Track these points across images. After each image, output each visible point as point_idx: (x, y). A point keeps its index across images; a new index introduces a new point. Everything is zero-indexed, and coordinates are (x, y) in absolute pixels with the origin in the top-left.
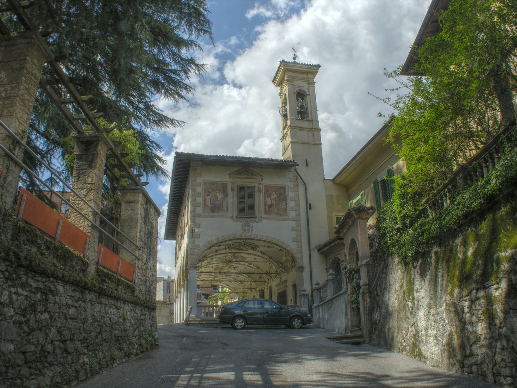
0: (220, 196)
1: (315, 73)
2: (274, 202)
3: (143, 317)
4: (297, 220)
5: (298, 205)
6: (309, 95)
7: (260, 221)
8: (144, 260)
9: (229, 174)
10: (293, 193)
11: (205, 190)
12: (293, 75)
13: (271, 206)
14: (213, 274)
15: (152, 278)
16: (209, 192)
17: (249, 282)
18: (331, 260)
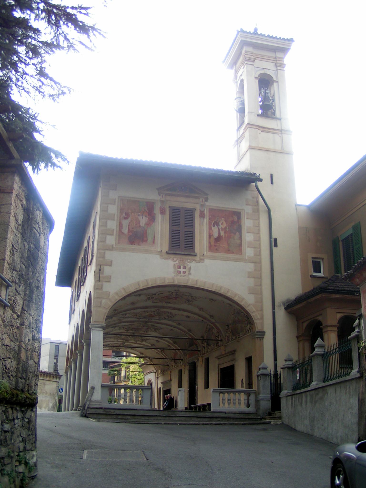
0: (143, 220)
1: (285, 50)
2: (222, 233)
3: (7, 427)
4: (257, 262)
5: (259, 239)
6: (277, 82)
7: (201, 260)
8: (18, 309)
9: (158, 189)
10: (252, 221)
11: (121, 210)
12: (256, 52)
13: (218, 239)
14: (123, 337)
15: (33, 345)
16: (127, 214)
17: (174, 351)
18: (305, 324)
